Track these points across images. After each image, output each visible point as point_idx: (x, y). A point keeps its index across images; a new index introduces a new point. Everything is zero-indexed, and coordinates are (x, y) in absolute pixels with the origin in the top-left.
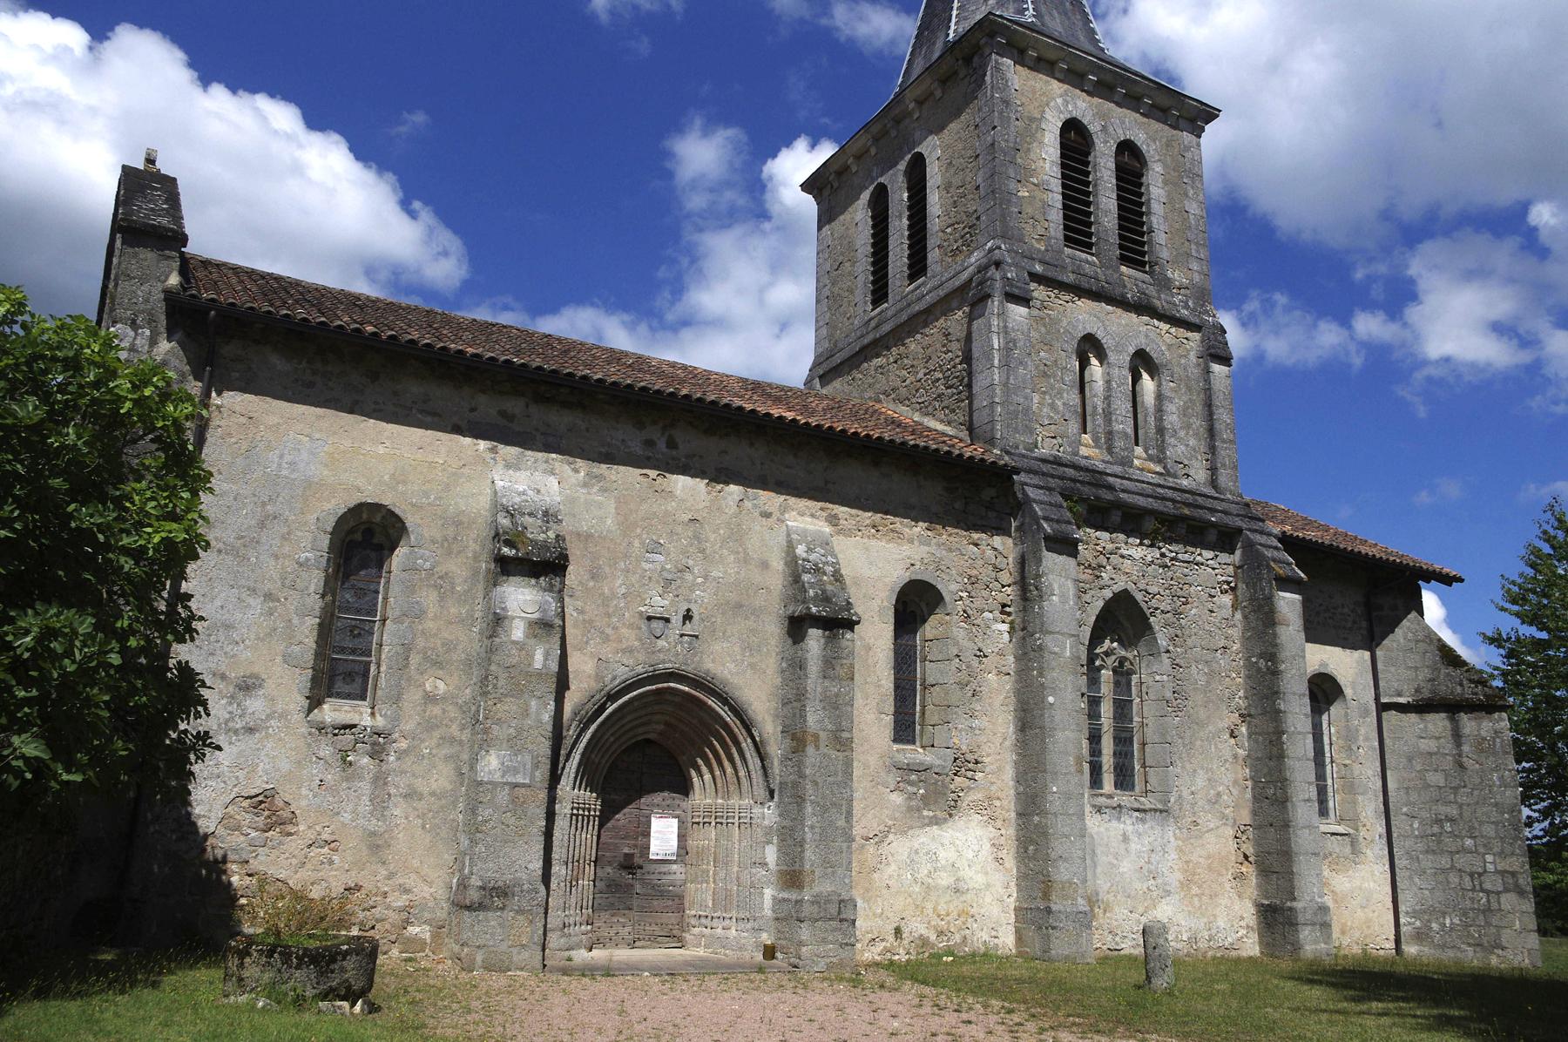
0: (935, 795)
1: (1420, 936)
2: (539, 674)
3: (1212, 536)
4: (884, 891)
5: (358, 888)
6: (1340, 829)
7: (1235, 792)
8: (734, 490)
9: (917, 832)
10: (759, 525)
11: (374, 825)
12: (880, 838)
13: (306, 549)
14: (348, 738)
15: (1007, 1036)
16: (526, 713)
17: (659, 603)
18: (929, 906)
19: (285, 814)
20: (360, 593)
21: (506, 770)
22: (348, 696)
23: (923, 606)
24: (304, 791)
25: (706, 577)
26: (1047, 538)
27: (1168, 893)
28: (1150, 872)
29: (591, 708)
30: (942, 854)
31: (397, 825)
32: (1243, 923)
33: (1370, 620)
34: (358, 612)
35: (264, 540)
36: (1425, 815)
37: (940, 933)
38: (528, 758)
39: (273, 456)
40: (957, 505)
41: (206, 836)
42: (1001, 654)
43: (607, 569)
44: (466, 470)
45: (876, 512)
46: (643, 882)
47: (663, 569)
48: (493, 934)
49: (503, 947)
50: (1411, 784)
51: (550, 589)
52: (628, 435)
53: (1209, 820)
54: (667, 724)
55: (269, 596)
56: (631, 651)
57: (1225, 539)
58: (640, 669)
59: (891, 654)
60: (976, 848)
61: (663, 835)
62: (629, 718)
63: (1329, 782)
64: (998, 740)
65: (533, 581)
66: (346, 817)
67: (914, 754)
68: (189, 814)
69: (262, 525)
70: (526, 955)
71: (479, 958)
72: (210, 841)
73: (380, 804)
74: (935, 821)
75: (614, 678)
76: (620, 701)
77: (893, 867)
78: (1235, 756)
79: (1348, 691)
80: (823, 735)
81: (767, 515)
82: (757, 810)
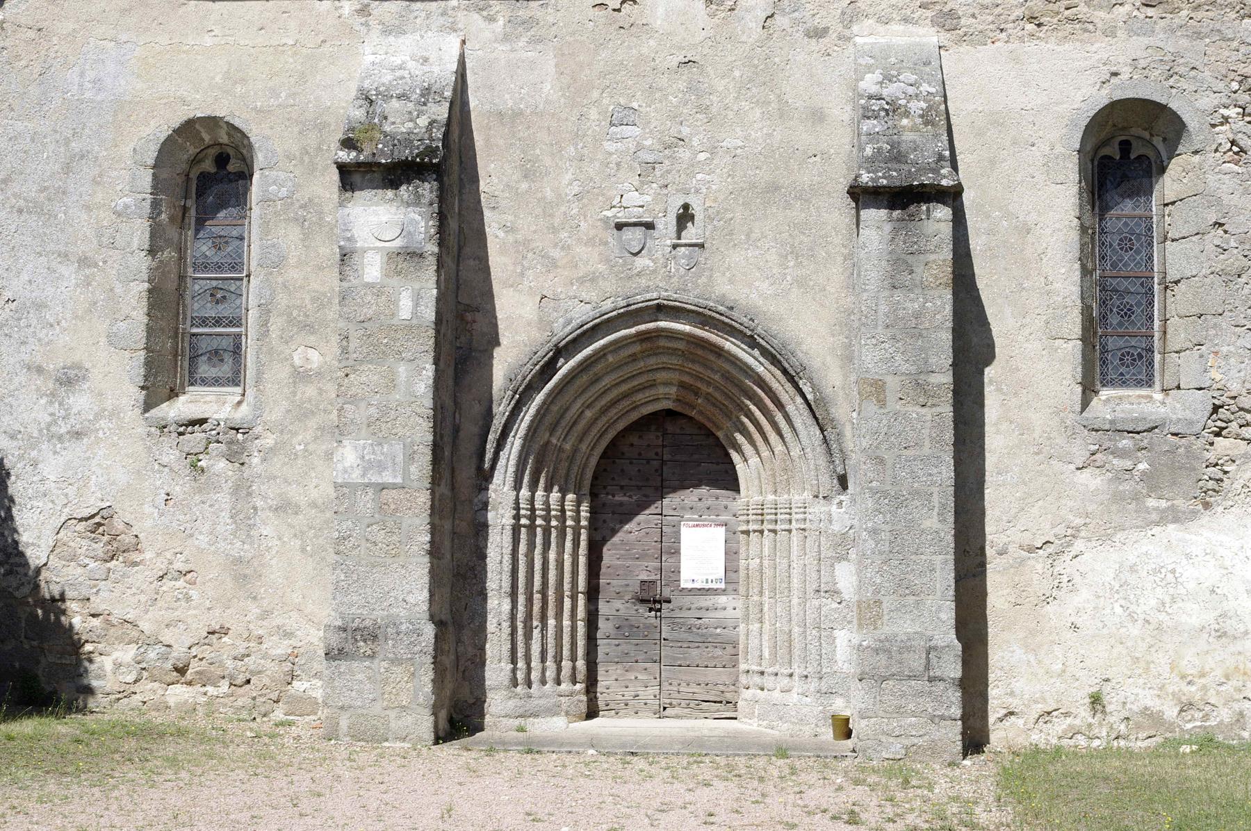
2: (409, 328)
4: (1069, 634)
5: (224, 631)
9: (1134, 535)
11: (236, 549)
13: (121, 192)
14: (197, 437)
16: (392, 384)
17: (636, 201)
18: (1162, 661)
19: (127, 539)
20: (220, 243)
21: (368, 466)
22: (216, 382)
23: (1157, 141)
24: (148, 509)
25: (713, 151)
29: (531, 370)
30: (1189, 573)
31: (269, 549)
34: (219, 267)
35: (71, 188)
37: (1186, 707)
38: (398, 448)
39: (73, 76)
41: (38, 571)
43: (547, 161)
44: (326, 48)
46: (675, 624)
47: (640, 147)
48: (360, 692)
49: (377, 708)
51: (417, 200)
54: (682, 385)
55: (84, 262)
56: (593, 280)
58: (608, 305)
59: (1074, 236)
61: (700, 551)
62: (606, 381)
65: (390, 193)
66: (202, 540)
67: (1114, 402)
68: (16, 543)
69: (67, 169)
70: (409, 719)
71: (344, 723)
72: (44, 575)
73: (244, 521)
74: (1173, 516)
75: (569, 322)
76: (580, 357)
80: (892, 383)
81: (818, 33)
82: (818, 509)
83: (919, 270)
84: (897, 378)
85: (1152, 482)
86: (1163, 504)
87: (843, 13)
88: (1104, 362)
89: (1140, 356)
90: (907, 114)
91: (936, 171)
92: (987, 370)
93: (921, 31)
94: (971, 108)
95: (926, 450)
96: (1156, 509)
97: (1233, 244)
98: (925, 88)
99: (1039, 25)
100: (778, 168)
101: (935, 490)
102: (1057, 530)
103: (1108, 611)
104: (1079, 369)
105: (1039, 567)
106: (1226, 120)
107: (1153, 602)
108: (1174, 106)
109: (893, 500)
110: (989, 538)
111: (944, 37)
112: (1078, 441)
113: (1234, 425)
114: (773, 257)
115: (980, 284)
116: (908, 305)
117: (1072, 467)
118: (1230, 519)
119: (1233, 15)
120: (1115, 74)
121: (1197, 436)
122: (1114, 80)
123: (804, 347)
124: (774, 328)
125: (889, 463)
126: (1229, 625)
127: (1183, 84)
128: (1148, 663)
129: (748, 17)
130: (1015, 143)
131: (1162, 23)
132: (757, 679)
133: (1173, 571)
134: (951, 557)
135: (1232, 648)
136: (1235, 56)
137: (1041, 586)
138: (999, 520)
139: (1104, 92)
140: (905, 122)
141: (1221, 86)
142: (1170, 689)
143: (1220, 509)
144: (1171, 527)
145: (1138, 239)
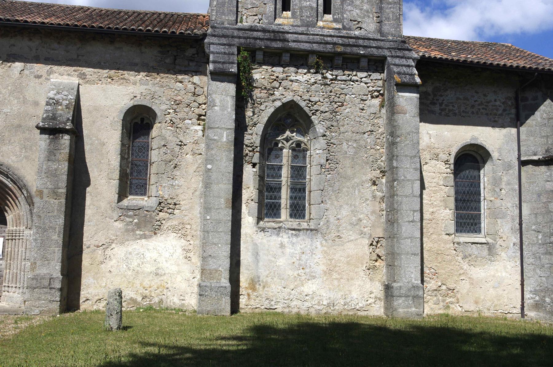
0: (147, 224)
1: (537, 306)
3: (364, 63)
4: (108, 274)
6: (483, 240)
7: (373, 218)
8: (18, 65)
9: (131, 242)
10: (34, 82)
12: (105, 246)
15: (1, 352)
18: (138, 282)
23: (151, 118)
26: (397, 85)
27: (314, 277)
28: (300, 265)
30: (148, 255)
32: (372, 296)
33: (517, 108)
36: (546, 230)
40: (168, 61)
42: (196, 143)
45: (111, 69)
50: (539, 211)
52: (128, 52)
53: (350, 234)
57: (376, 64)
60: (172, 251)
63: (482, 212)
64: (190, 192)
67: (132, 200)
74: (145, 237)
77: (114, 261)
78: (374, 197)
79: (495, 155)
80: (46, 191)
81: (39, 77)
83: (58, 155)
84: (47, 190)
85: (138, 226)
86: (142, 233)
87: (48, 71)
88: (131, 187)
89: (143, 186)
90: (61, 105)
91: (65, 124)
92: (87, 189)
93: (73, 79)
94: (88, 104)
95: (55, 214)
96: (139, 234)
97: (169, 152)
98: (70, 97)
99: (112, 80)
100: (21, 120)
101: (57, 226)
102: (107, 241)
103: (121, 267)
104: (118, 189)
105: (100, 252)
106: (169, 113)
107: (136, 264)
108: (153, 108)
109: (43, 230)
110: (84, 242)
111: (81, 81)
112: (116, 212)
113: (165, 209)
114: (17, 149)
115: (87, 161)
116: (53, 166)
117: (113, 220)
118: (162, 238)
119: (173, 81)
120: (135, 97)
121: (154, 211)
122: (135, 99)
123: (26, 179)
124: (16, 172)
125: (42, 218)
126: (160, 272)
127: (157, 101)
128: (133, 283)
129: (15, 70)
130: (101, 116)
131: (151, 82)
132: (6, 289)
133: (143, 254)
134: (61, 248)
135: (160, 279)
136: (173, 94)
137: (100, 258)
138: (88, 237)
139: (132, 102)
140: (60, 107)
141: (168, 102)
142: (140, 292)
143: (159, 235)
144: (143, 240)
145: (144, 149)
